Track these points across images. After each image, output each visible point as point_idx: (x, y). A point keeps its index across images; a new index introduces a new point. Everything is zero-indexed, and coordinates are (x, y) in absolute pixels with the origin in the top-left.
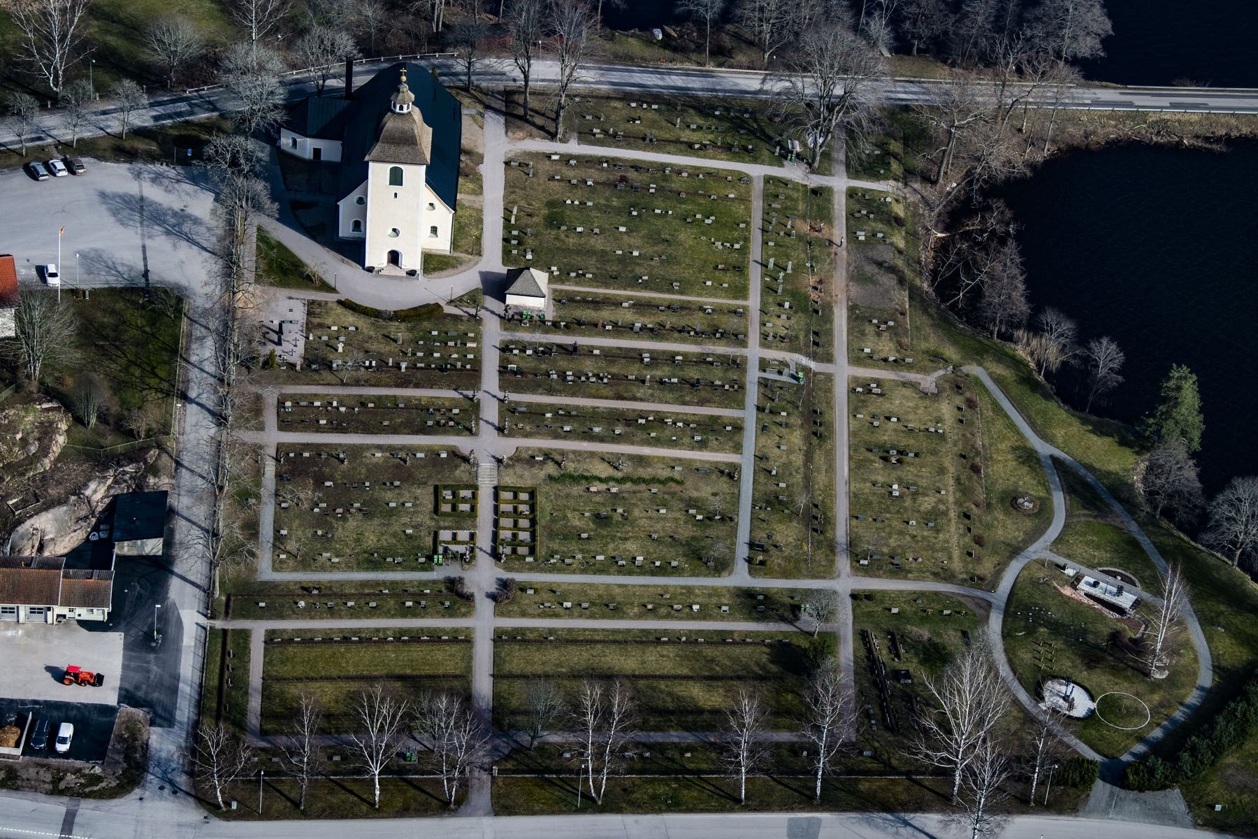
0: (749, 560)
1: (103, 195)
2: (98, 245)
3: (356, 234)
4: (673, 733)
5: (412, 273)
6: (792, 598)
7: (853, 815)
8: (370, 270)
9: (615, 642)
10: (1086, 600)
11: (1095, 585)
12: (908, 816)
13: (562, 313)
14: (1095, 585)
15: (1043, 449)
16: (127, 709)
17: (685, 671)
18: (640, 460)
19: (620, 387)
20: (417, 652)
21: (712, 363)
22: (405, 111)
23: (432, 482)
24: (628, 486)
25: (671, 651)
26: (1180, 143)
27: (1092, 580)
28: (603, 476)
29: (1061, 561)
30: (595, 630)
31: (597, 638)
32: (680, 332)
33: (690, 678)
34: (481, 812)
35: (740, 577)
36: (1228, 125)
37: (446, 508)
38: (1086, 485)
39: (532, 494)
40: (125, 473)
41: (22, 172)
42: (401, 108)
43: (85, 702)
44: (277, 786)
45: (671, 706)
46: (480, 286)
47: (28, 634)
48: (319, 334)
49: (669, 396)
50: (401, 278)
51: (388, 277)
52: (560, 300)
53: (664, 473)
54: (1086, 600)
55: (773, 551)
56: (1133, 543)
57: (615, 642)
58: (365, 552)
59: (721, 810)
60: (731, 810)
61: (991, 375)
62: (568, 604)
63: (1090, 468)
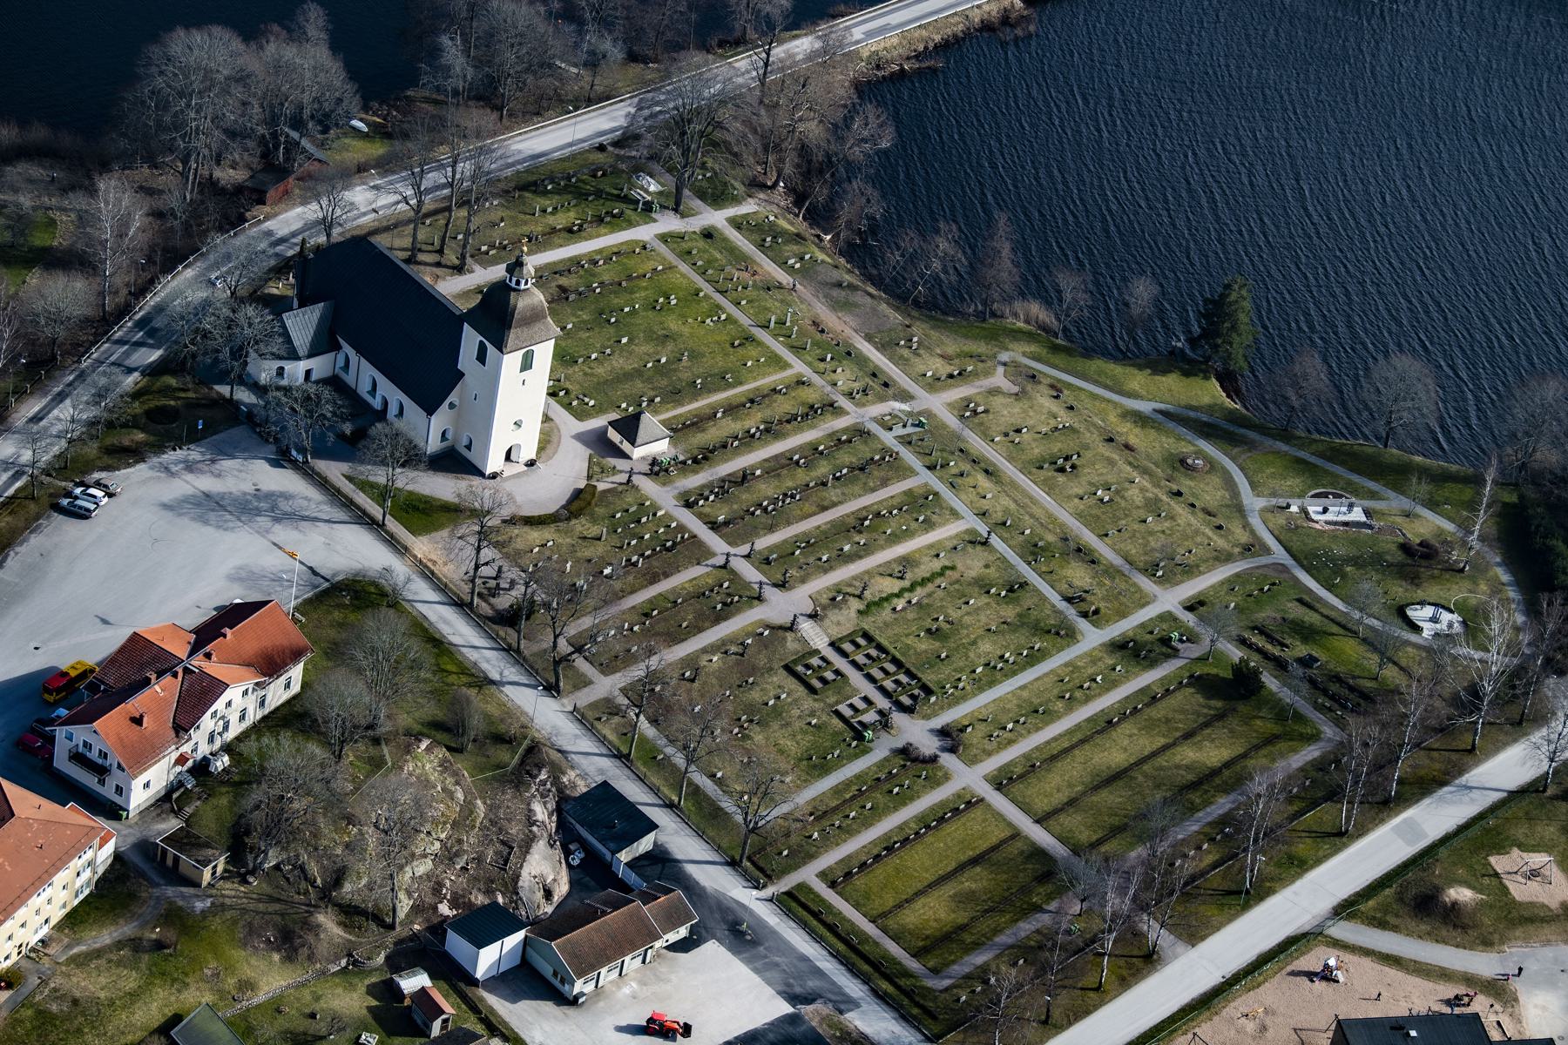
0: (1085, 615)
1: (166, 506)
2: (238, 562)
3: (445, 444)
4: (1221, 801)
5: (531, 464)
6: (1151, 633)
7: (1426, 801)
8: (494, 476)
9: (1083, 742)
10: (1327, 527)
11: (1325, 511)
12: (1463, 780)
13: (681, 447)
14: (1325, 511)
15: (1145, 407)
16: (807, 1010)
17: (1161, 741)
18: (907, 562)
19: (813, 495)
20: (954, 830)
21: (850, 441)
22: (523, 287)
23: (777, 665)
24: (920, 592)
25: (1127, 728)
26: (902, 70)
27: (1320, 509)
28: (896, 591)
29: (1282, 502)
30: (1055, 739)
31: (1066, 745)
32: (788, 422)
33: (1174, 744)
34: (774, 974)
35: (1092, 637)
36: (921, 39)
37: (817, 684)
38: (1206, 424)
39: (866, 635)
40: (543, 783)
41: (58, 518)
42: (518, 283)
43: (768, 1020)
44: (1461, 990)
45: (1191, 777)
46: (589, 451)
47: (643, 983)
48: (838, 546)
49: (857, 489)
50: (518, 475)
51: (514, 476)
52: (678, 430)
53: (936, 565)
54: (1327, 527)
55: (1088, 597)
56: (1299, 461)
57: (1083, 742)
58: (800, 760)
59: (1336, 850)
60: (1345, 846)
61: (1024, 354)
62: (1010, 726)
63: (1191, 408)
